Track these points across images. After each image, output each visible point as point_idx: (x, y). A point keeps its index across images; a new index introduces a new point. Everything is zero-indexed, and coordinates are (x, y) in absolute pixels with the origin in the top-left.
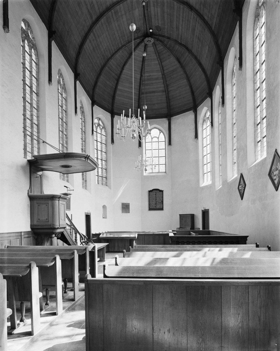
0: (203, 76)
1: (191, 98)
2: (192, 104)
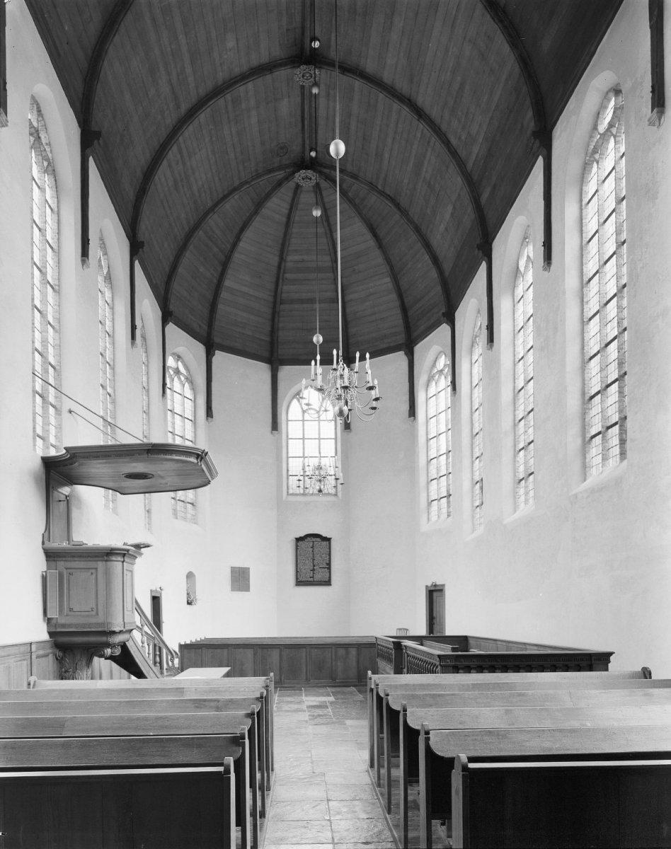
0: (434, 274)
1: (399, 321)
2: (404, 335)
